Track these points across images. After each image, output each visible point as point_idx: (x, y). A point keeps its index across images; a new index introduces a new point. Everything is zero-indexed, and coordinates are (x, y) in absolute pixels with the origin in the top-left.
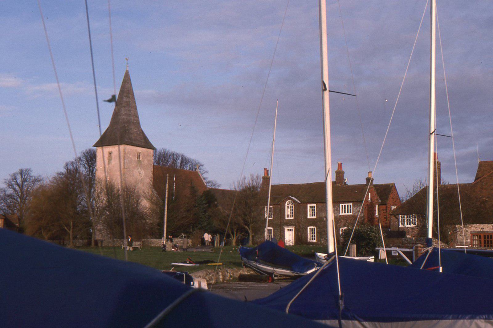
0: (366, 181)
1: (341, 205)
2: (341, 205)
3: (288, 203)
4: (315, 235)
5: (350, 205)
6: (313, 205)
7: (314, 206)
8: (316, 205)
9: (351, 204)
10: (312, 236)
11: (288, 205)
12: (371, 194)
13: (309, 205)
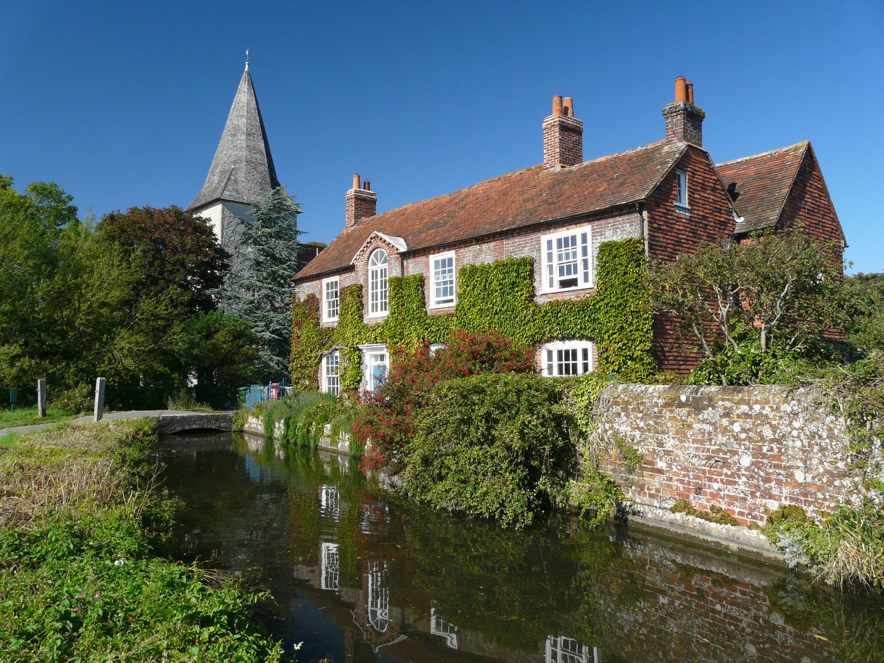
5: (584, 236)
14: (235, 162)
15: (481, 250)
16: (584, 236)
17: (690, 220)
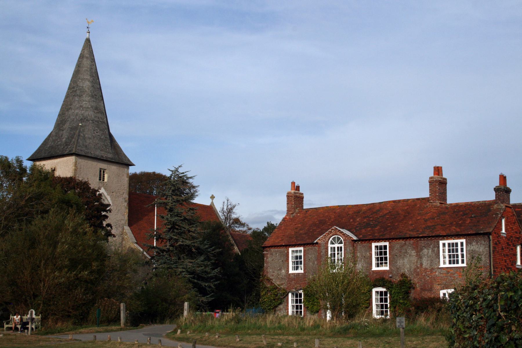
0: (494, 193)
1: (441, 242)
2: (441, 242)
3: (331, 241)
4: (301, 306)
5: (462, 244)
6: (382, 244)
7: (385, 247)
8: (390, 243)
9: (464, 241)
10: (297, 308)
11: (333, 246)
12: (506, 221)
13: (374, 245)
14: (81, 120)
15: (405, 244)
16: (462, 244)
17: (506, 238)
